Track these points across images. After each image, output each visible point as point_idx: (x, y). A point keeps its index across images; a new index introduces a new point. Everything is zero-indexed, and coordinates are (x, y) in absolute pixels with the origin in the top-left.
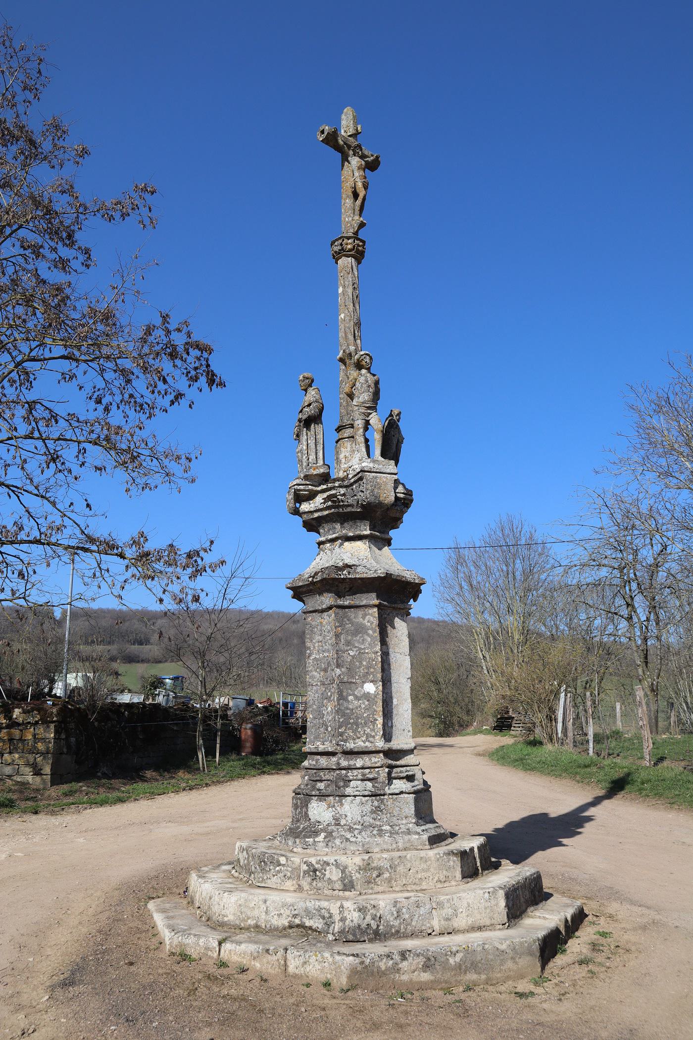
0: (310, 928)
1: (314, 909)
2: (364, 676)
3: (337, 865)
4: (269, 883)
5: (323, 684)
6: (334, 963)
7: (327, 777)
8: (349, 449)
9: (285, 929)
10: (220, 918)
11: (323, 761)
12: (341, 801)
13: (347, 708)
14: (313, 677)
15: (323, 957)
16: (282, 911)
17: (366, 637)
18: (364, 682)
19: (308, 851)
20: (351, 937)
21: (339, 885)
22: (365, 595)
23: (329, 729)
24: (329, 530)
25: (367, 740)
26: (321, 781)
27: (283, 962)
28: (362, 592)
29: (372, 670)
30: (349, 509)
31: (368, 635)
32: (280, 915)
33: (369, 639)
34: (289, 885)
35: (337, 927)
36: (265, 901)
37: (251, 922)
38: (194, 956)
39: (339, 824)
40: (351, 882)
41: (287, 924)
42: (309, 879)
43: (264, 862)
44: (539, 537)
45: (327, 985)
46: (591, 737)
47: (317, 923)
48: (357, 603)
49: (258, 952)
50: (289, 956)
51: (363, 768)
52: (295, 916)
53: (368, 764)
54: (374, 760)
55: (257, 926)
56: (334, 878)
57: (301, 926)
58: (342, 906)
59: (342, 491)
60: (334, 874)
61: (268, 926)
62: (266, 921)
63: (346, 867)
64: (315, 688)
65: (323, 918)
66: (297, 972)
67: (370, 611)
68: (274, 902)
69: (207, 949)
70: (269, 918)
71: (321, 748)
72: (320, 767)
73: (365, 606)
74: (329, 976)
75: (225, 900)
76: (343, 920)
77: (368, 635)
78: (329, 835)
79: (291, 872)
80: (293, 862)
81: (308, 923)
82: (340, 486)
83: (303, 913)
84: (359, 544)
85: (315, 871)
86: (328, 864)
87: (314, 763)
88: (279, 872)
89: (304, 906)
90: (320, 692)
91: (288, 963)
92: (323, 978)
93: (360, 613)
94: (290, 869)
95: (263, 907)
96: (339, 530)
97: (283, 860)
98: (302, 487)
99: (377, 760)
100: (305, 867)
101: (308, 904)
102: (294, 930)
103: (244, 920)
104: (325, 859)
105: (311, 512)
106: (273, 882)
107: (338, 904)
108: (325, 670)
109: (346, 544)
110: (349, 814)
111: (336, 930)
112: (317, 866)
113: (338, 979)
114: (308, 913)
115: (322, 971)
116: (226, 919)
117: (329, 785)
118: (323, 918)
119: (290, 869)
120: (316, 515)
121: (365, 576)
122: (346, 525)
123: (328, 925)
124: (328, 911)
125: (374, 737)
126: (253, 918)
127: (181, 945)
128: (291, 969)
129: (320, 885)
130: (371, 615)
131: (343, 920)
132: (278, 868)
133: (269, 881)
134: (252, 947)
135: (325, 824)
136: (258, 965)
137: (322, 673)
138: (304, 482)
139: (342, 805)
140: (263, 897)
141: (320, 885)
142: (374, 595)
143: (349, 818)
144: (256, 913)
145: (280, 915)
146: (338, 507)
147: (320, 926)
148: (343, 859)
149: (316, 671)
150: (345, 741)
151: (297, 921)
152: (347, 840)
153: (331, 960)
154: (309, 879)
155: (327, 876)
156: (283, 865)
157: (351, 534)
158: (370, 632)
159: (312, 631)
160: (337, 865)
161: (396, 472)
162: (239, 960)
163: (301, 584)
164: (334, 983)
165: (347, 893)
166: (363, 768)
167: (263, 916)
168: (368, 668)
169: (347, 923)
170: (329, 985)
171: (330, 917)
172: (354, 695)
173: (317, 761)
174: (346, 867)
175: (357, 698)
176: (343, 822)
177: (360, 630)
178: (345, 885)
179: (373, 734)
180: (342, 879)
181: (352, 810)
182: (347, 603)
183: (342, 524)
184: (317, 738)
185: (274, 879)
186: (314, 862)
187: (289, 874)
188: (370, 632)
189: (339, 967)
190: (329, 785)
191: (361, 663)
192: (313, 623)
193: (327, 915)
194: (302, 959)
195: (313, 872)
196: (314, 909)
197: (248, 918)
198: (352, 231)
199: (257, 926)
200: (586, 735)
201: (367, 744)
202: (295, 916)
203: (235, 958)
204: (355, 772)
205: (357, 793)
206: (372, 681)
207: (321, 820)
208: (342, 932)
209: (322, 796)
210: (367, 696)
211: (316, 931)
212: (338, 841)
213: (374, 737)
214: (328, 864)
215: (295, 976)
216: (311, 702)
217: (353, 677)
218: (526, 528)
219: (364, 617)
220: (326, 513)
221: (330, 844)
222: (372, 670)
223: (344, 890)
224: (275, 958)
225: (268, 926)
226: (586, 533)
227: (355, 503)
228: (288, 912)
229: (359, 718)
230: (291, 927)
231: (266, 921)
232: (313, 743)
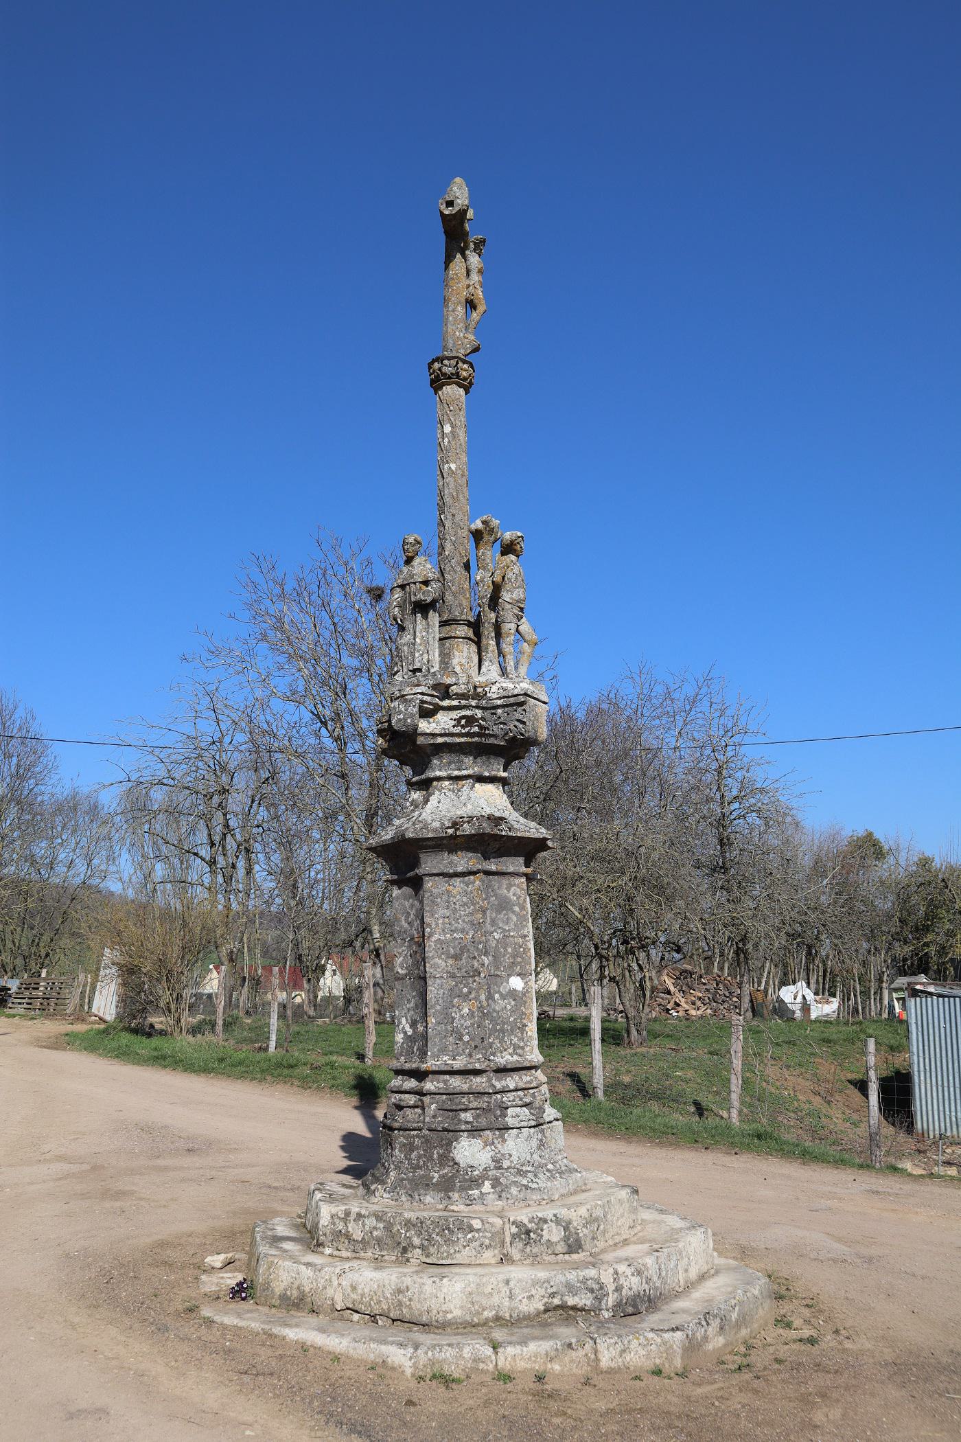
0: (574, 1308)
1: (578, 1281)
2: (510, 967)
3: (558, 1221)
4: (459, 1258)
5: (453, 976)
6: (664, 1343)
7: (474, 1104)
8: (465, 654)
9: (538, 1314)
10: (440, 1317)
11: (456, 1083)
12: (502, 1137)
13: (494, 1011)
14: (436, 966)
15: (647, 1339)
16: (533, 1292)
17: (511, 915)
18: (509, 976)
19: (476, 1207)
20: (630, 1310)
21: (561, 1248)
22: (511, 859)
23: (466, 1038)
24: (449, 763)
25: (515, 1053)
26: (465, 1110)
27: (593, 1356)
28: (509, 854)
29: (519, 959)
30: (491, 741)
31: (514, 912)
32: (530, 1297)
33: (515, 919)
34: (490, 1256)
35: (611, 1300)
36: (507, 1282)
37: (488, 1314)
38: (456, 1375)
39: (500, 1168)
40: (578, 1241)
41: (542, 1308)
42: (521, 1245)
43: (449, 1229)
44: (35, 729)
45: (657, 1372)
46: (220, 1022)
47: (584, 1300)
48: (504, 869)
49: (557, 1350)
50: (601, 1346)
51: (516, 1090)
52: (553, 1295)
53: (521, 1085)
54: (526, 1078)
55: (498, 1318)
56: (555, 1239)
57: (563, 1307)
58: (616, 1273)
59: (479, 714)
60: (554, 1234)
61: (515, 1315)
62: (511, 1309)
63: (569, 1222)
64: (438, 981)
65: (592, 1291)
66: (613, 1365)
67: (517, 881)
68: (519, 1281)
69: (477, 1360)
70: (515, 1304)
71: (458, 1064)
72: (451, 1091)
73: (511, 874)
74: (658, 1361)
75: (445, 1290)
76: (618, 1289)
77: (514, 912)
78: (496, 1183)
79: (491, 1239)
80: (492, 1225)
81: (571, 1301)
82: (477, 707)
83: (564, 1290)
84: (490, 787)
85: (528, 1232)
86: (545, 1221)
87: (441, 1085)
88: (471, 1240)
89: (563, 1279)
90: (447, 987)
91: (600, 1356)
92: (649, 1365)
93: (505, 881)
94: (488, 1235)
95: (505, 1290)
96: (471, 766)
97: (477, 1224)
98: (428, 699)
99: (528, 1078)
100: (514, 1230)
101: (569, 1277)
102: (550, 1314)
103: (478, 1313)
104: (540, 1215)
105: (433, 735)
106: (464, 1255)
107: (611, 1271)
108: (457, 957)
109: (477, 785)
110: (514, 1153)
111: (610, 1304)
112: (530, 1226)
113: (671, 1362)
114: (571, 1289)
115: (648, 1357)
116: (449, 1316)
117: (478, 1116)
118: (592, 1291)
119: (488, 1235)
120: (440, 740)
121: (527, 835)
122: (478, 760)
123: (599, 1299)
124: (598, 1281)
125: (523, 1048)
126: (491, 1308)
127: (432, 1363)
128: (605, 1362)
129: (535, 1250)
130: (518, 886)
131: (618, 1289)
132: (469, 1236)
133: (458, 1255)
134: (546, 1346)
135: (481, 1169)
136: (557, 1367)
137: (450, 962)
138: (430, 692)
139: (504, 1141)
140: (501, 1277)
141: (535, 1250)
142: (521, 860)
143: (515, 1158)
144: (495, 1300)
145: (530, 1297)
146: (484, 735)
147: (588, 1303)
148: (564, 1213)
149: (440, 957)
150: (494, 1054)
151: (556, 1301)
152: (527, 1187)
153: (659, 1340)
154: (521, 1245)
155: (546, 1237)
156: (478, 1231)
157: (486, 774)
158: (517, 909)
159: (433, 901)
160: (558, 1221)
161: (546, 700)
162: (528, 1366)
163: (430, 835)
164: (667, 1369)
165: (575, 1256)
166: (516, 1090)
167: (506, 1303)
168: (514, 956)
169: (624, 1292)
170: (661, 1371)
171: (601, 1288)
172: (499, 992)
173: (445, 1082)
174: (569, 1222)
175: (503, 997)
176: (506, 1164)
177: (504, 905)
178: (569, 1246)
179: (522, 1044)
180: (566, 1239)
181: (517, 1146)
182: (494, 868)
183: (475, 758)
184: (443, 1051)
185: (466, 1251)
186: (526, 1221)
187: (487, 1242)
188: (517, 909)
189: (671, 1347)
190: (478, 1116)
191: (506, 950)
192: (435, 891)
193: (596, 1287)
194: (619, 1347)
195: (525, 1234)
196: (578, 1281)
197: (484, 1310)
198: (462, 351)
199: (498, 1318)
200: (214, 1013)
201: (516, 1058)
202: (553, 1295)
203: (522, 1365)
204: (511, 1096)
205: (523, 1124)
206: (519, 975)
207: (475, 1164)
208: (618, 1305)
209: (475, 1131)
210: (513, 994)
211: (582, 1310)
212: (514, 1190)
213: (523, 1048)
214: (545, 1221)
215: (610, 1371)
216: (433, 1001)
217: (498, 968)
218: (20, 713)
219: (508, 889)
220: (462, 740)
221: (504, 1195)
222: (519, 959)
223: (570, 1252)
224: (581, 1353)
225: (515, 1315)
226: (170, 739)
227: (501, 733)
228: (542, 1292)
229: (504, 1024)
230: (546, 1311)
231: (511, 1309)
232: (436, 1057)
